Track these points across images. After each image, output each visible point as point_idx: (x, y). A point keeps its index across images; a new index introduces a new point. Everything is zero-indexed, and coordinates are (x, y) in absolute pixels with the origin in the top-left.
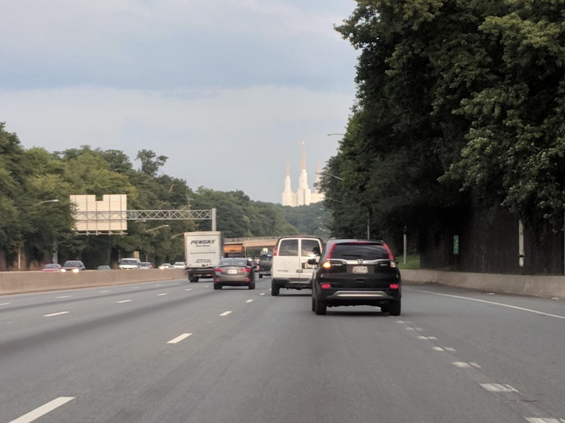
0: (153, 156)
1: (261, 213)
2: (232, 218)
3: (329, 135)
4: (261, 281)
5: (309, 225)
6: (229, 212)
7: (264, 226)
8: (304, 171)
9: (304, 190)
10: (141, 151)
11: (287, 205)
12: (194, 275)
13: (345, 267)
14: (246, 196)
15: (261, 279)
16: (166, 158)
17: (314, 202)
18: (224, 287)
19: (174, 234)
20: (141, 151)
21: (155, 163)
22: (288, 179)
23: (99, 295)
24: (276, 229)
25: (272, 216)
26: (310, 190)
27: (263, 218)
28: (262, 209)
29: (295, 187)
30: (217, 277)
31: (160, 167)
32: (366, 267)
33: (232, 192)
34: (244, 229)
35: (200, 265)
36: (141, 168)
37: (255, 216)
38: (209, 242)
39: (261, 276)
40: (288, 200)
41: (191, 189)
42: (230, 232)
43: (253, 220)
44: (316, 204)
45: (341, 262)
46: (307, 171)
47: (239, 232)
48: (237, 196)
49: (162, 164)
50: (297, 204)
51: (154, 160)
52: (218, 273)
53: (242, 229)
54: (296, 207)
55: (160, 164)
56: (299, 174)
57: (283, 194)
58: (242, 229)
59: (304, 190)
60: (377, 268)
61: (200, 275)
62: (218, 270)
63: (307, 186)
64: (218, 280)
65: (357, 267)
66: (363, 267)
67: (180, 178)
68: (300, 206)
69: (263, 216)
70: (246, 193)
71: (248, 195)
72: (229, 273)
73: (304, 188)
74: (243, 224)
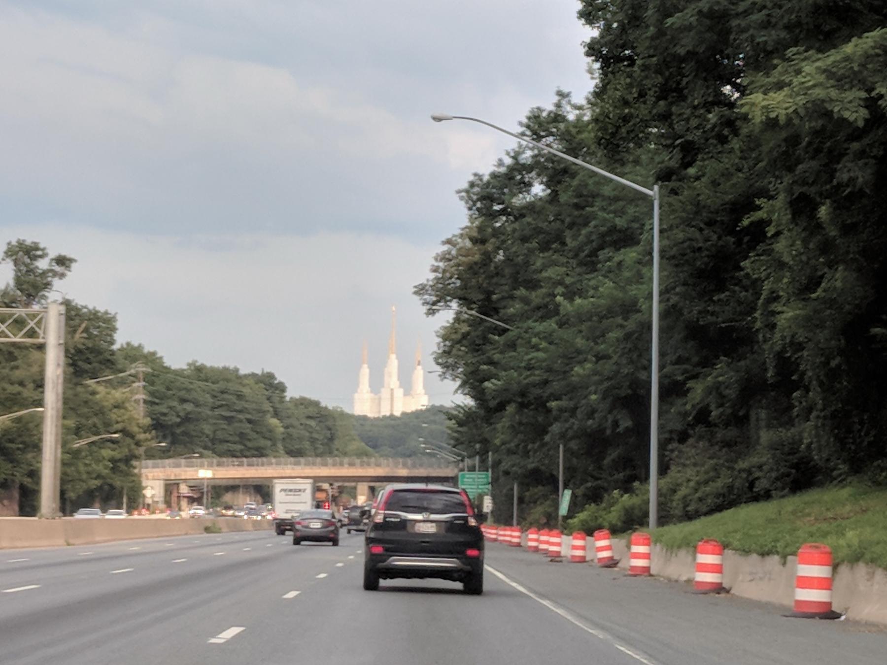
0: (41, 257)
1: (309, 417)
4: (295, 552)
5: (399, 449)
7: (313, 441)
8: (393, 357)
9: (392, 390)
10: (14, 243)
12: (282, 527)
13: (403, 524)
14: (281, 383)
15: (297, 547)
16: (71, 260)
17: (409, 411)
18: (303, 543)
19: (80, 438)
20: (14, 243)
21: (44, 273)
22: (365, 371)
24: (337, 450)
25: (329, 423)
26: (401, 391)
27: (311, 427)
28: (310, 409)
29: (377, 385)
30: (297, 530)
31: (56, 283)
32: (434, 524)
33: (254, 375)
34: (269, 443)
36: (12, 283)
37: (296, 423)
39: (349, 531)
40: (363, 405)
41: (161, 358)
42: (239, 447)
43: (290, 430)
44: (413, 413)
45: (397, 516)
46: (397, 358)
47: (258, 449)
48: (262, 382)
49: (62, 276)
50: (379, 412)
51: (42, 264)
52: (298, 527)
53: (263, 443)
55: (55, 274)
56: (384, 363)
57: (356, 396)
58: (263, 443)
59: (392, 390)
60: (450, 526)
61: (288, 527)
62: (299, 523)
63: (398, 383)
64: (298, 534)
65: (421, 524)
66: (429, 525)
67: (101, 309)
68: (385, 417)
69: (313, 423)
70: (280, 378)
71: (282, 380)
72: (312, 526)
73: (392, 387)
74: (268, 435)
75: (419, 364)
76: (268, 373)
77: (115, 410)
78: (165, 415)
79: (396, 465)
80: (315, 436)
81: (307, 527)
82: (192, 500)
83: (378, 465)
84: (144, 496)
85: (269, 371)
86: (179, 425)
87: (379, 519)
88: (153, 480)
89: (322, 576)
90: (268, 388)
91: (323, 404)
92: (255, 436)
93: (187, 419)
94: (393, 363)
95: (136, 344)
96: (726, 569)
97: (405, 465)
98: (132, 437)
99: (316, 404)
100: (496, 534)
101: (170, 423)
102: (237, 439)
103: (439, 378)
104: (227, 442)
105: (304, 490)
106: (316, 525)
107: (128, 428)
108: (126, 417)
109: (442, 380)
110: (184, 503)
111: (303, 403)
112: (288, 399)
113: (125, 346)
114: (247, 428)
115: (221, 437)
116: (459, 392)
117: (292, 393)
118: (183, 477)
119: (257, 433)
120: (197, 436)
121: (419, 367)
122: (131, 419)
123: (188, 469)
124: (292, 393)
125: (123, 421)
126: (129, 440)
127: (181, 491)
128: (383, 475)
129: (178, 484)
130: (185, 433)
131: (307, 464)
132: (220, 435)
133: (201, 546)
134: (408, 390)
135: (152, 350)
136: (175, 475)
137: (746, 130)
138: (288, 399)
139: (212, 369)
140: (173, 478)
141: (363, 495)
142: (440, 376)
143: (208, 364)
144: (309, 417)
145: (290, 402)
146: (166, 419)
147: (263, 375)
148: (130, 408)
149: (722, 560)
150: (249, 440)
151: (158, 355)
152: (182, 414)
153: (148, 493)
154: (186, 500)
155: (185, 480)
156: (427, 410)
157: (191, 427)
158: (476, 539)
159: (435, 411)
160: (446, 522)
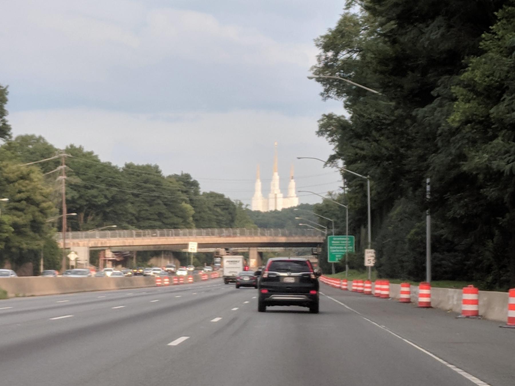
1: (216, 206)
2: (161, 202)
3: (299, 158)
6: (156, 194)
9: (276, 194)
11: (256, 210)
12: (228, 280)
13: (278, 278)
15: (238, 289)
22: (259, 185)
23: (56, 305)
29: (266, 191)
33: (176, 176)
34: (180, 220)
35: (230, 275)
38: (236, 261)
40: (258, 204)
41: (96, 156)
42: (158, 223)
44: (289, 209)
45: (275, 274)
46: (279, 175)
47: (174, 224)
50: (268, 208)
53: (176, 220)
54: (267, 213)
58: (176, 220)
59: (276, 194)
63: (279, 191)
64: (238, 283)
68: (271, 211)
73: (276, 192)
75: (292, 178)
76: (186, 174)
77: (21, 181)
78: (95, 197)
79: (276, 235)
80: (221, 218)
81: (241, 280)
82: (115, 263)
83: (263, 235)
84: (68, 259)
85: (186, 173)
86: (108, 205)
87: (265, 276)
88: (77, 248)
89: (235, 309)
90: (186, 184)
91: (226, 196)
92: (171, 215)
93: (113, 201)
94: (276, 176)
95: (77, 146)
96: (481, 303)
97: (284, 235)
98: (37, 205)
99: (222, 196)
100: (363, 286)
101: (99, 203)
102: (156, 217)
103: (321, 98)
104: (149, 219)
105: (239, 262)
106: (246, 279)
107: (33, 197)
108: (29, 187)
109: (325, 100)
110: (109, 265)
111: (212, 195)
112: (201, 193)
113: (70, 148)
114: (163, 209)
115: (144, 216)
116: (328, 165)
117: (204, 188)
118: (108, 245)
119: (172, 212)
120: (122, 214)
121: (293, 181)
122: (35, 189)
123: (112, 239)
124: (204, 188)
125: (28, 191)
126: (33, 208)
127: (107, 256)
128: (266, 241)
129: (104, 250)
130: (115, 212)
131: (208, 234)
132: (143, 214)
133: (162, 293)
134: (285, 190)
135: (89, 150)
136: (102, 243)
137: (351, 203)
138: (201, 193)
139: (138, 167)
140: (99, 245)
141: (253, 258)
142: (322, 94)
143: (136, 164)
144: (216, 206)
145: (203, 195)
146: (97, 200)
147: (182, 175)
148: (36, 180)
149: (478, 297)
150: (166, 218)
151: (95, 154)
152: (109, 196)
153: (72, 257)
154: (110, 262)
155: (110, 247)
156: (298, 207)
157: (118, 207)
158: (316, 285)
159: (303, 207)
160: (299, 277)
